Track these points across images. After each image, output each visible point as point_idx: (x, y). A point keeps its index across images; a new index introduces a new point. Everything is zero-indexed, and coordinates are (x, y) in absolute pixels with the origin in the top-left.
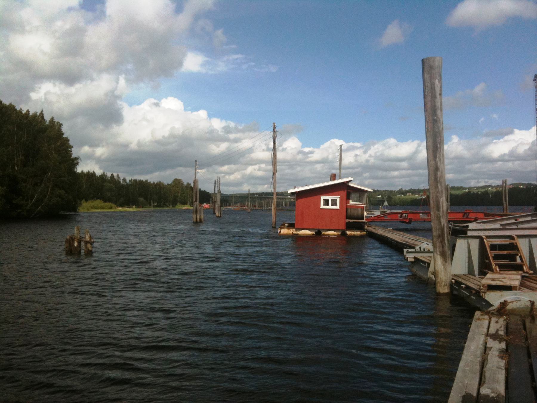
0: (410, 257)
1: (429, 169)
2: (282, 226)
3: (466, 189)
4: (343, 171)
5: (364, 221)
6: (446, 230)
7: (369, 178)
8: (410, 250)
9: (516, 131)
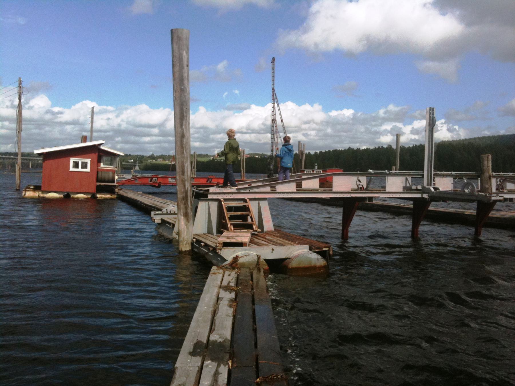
0: (158, 219)
1: (176, 136)
2: (27, 188)
3: (210, 156)
4: (95, 134)
5: (115, 184)
6: (189, 194)
7: (122, 142)
8: (157, 212)
9: (253, 106)
